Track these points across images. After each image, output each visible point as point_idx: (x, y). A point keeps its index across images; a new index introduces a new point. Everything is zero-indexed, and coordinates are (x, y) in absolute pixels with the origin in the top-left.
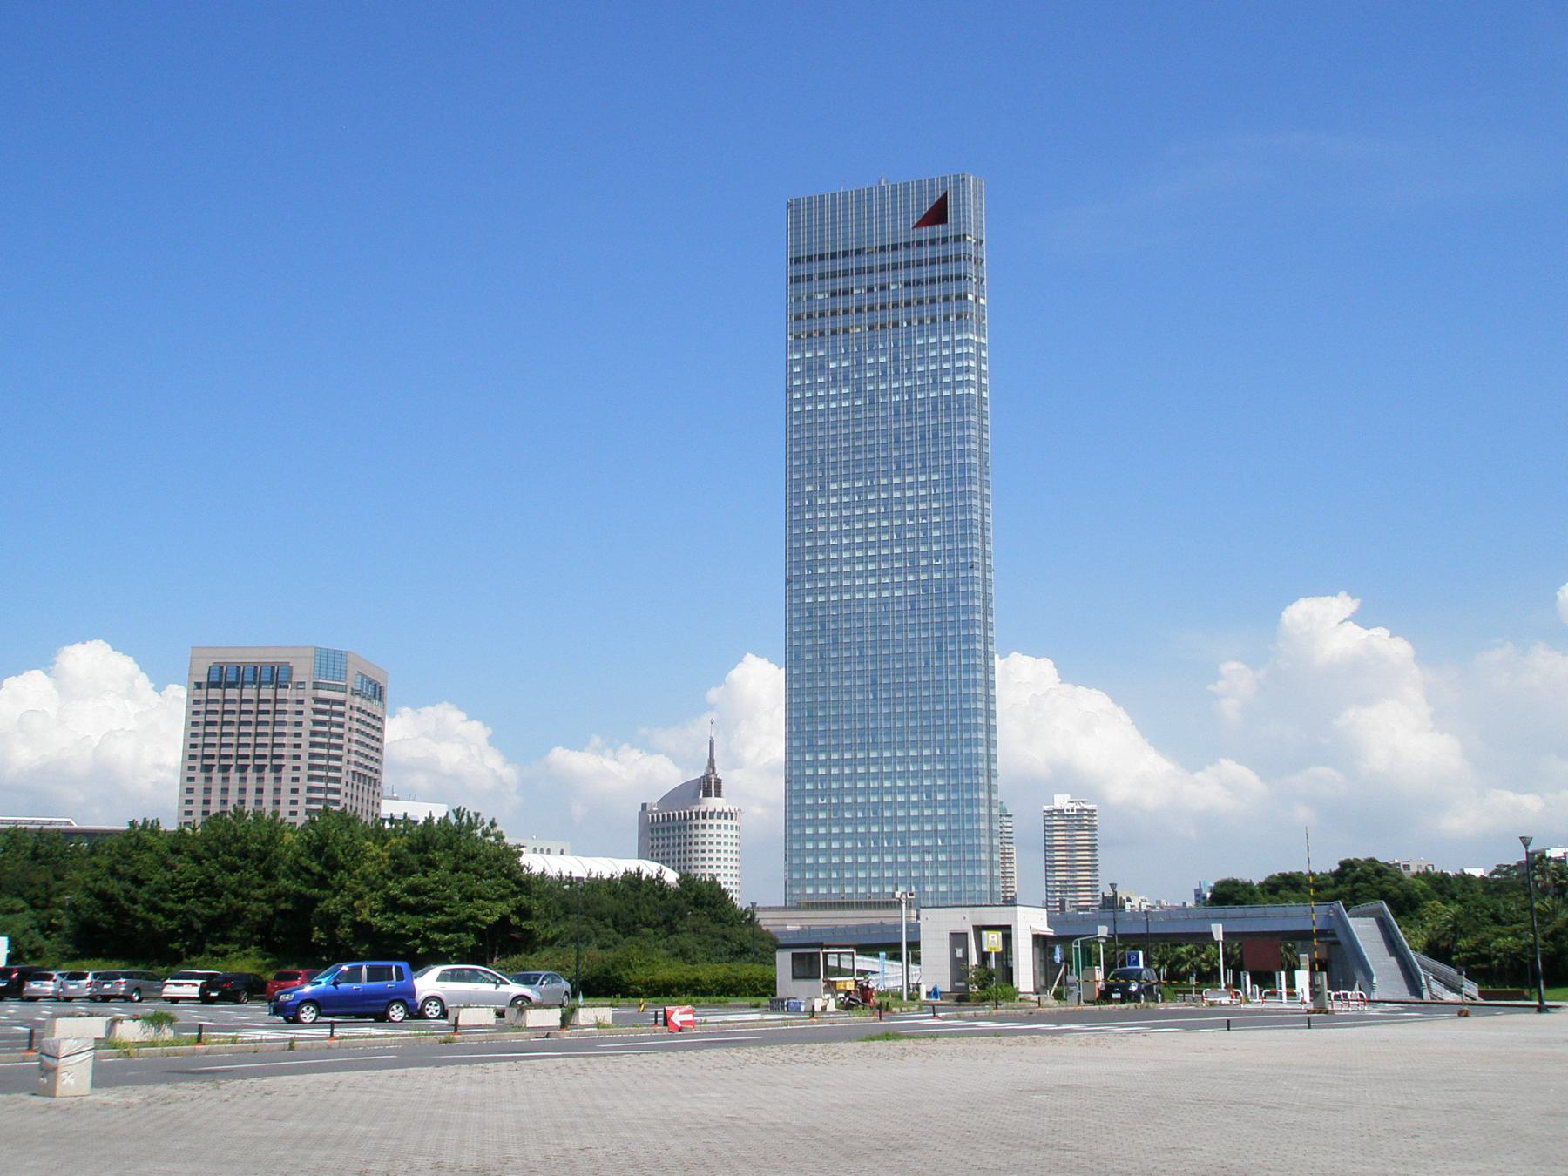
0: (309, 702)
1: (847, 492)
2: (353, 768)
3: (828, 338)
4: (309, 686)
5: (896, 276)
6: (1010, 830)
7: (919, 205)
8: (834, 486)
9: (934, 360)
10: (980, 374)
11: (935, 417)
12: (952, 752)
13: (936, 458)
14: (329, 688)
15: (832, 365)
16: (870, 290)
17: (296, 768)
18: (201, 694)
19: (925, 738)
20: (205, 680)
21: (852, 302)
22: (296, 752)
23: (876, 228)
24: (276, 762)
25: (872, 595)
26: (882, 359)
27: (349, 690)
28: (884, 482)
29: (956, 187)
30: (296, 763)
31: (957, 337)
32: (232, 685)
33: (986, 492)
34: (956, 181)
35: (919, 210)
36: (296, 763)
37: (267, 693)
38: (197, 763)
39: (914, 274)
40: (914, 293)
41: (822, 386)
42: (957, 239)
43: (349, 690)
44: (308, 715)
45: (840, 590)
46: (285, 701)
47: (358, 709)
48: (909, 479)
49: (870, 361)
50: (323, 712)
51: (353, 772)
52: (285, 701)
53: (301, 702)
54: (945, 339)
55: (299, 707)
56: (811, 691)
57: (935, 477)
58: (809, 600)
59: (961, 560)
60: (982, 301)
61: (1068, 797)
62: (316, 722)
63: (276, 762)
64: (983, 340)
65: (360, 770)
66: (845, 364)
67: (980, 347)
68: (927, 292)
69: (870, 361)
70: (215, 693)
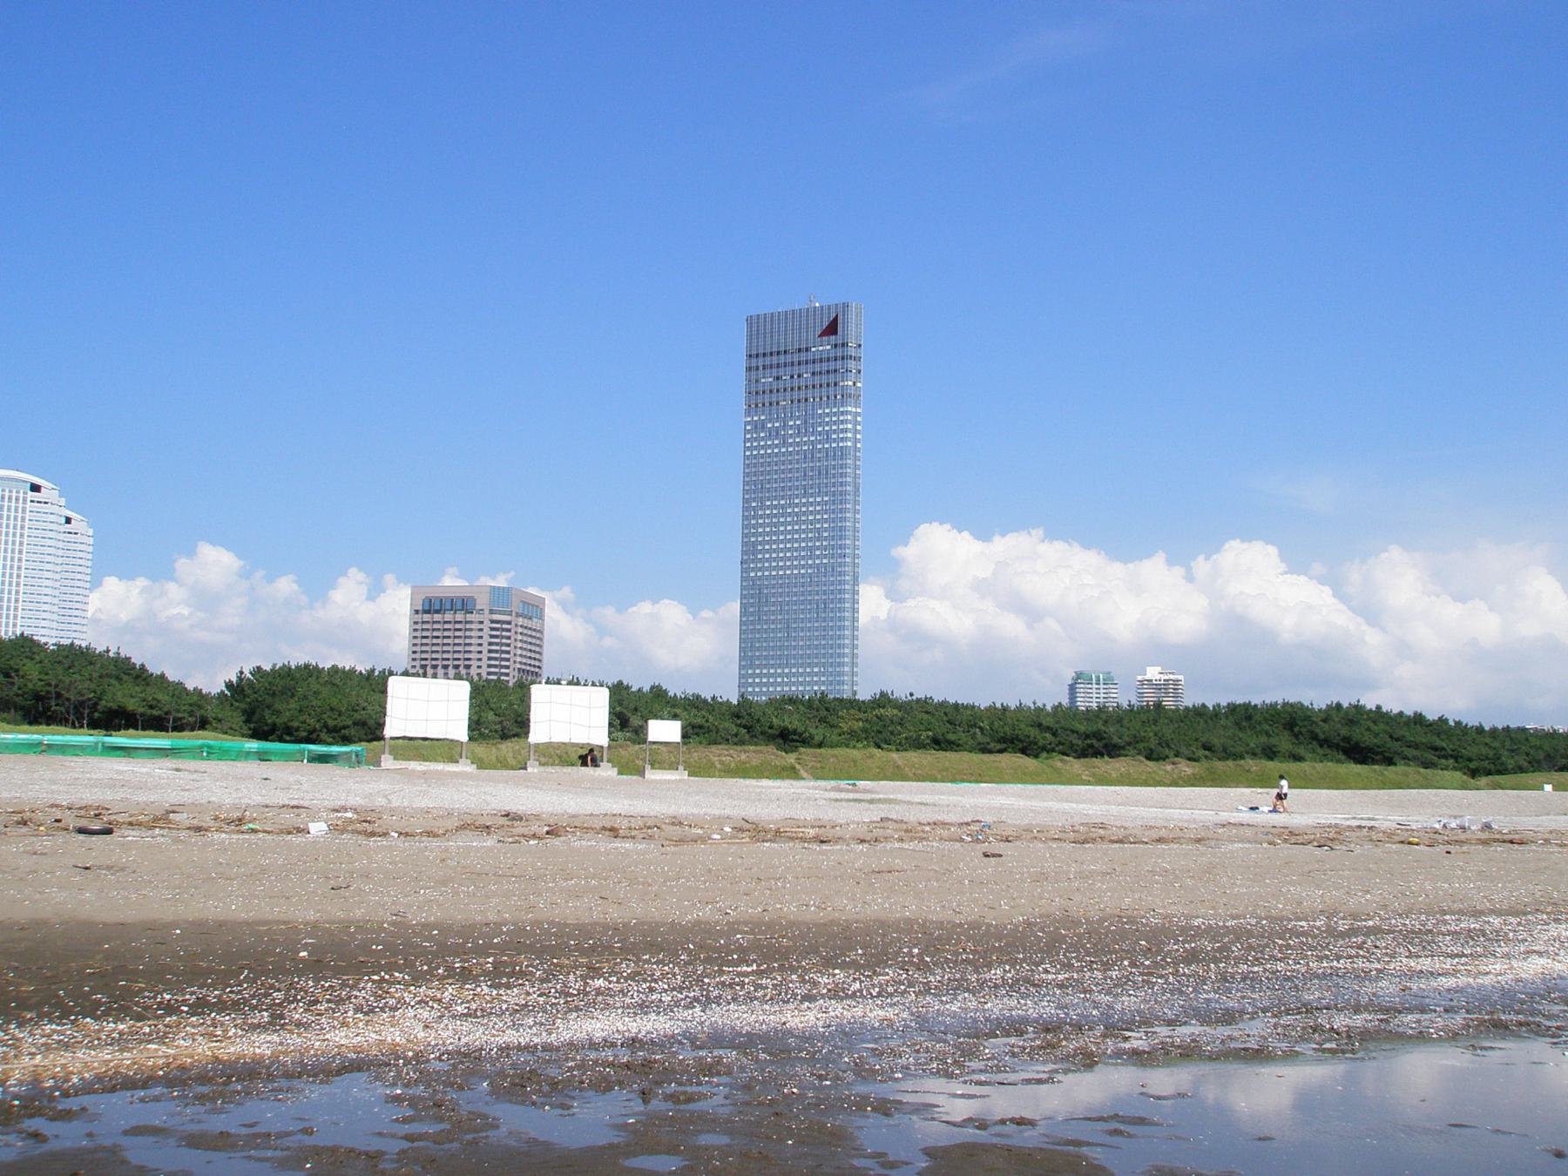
0: (487, 623)
1: (775, 507)
2: (519, 666)
3: (767, 409)
4: (487, 612)
5: (807, 369)
6: (1115, 695)
7: (822, 322)
8: (768, 503)
9: (827, 424)
10: (856, 432)
11: (827, 460)
12: (830, 670)
13: (827, 487)
14: (500, 613)
15: (769, 425)
16: (792, 377)
17: (479, 667)
18: (418, 618)
19: (815, 661)
20: (420, 608)
21: (781, 385)
22: (479, 656)
23: (796, 338)
24: (467, 663)
25: (788, 572)
26: (798, 422)
27: (514, 614)
28: (796, 501)
29: (844, 311)
30: (479, 663)
31: (841, 409)
32: (437, 612)
33: (857, 507)
34: (844, 308)
35: (822, 326)
36: (479, 663)
37: (459, 617)
38: (417, 663)
39: (817, 368)
40: (817, 380)
41: (763, 439)
42: (843, 345)
43: (514, 614)
44: (487, 631)
45: (770, 568)
46: (471, 622)
47: (521, 626)
48: (811, 500)
49: (791, 423)
50: (497, 629)
51: (519, 669)
52: (471, 622)
53: (482, 622)
54: (834, 410)
55: (481, 626)
56: (752, 631)
57: (826, 499)
58: (752, 574)
59: (839, 551)
60: (859, 385)
61: (1159, 669)
62: (492, 636)
63: (467, 663)
64: (859, 410)
65: (524, 667)
66: (777, 425)
67: (857, 414)
68: (824, 379)
69: (791, 423)
70: (427, 617)
